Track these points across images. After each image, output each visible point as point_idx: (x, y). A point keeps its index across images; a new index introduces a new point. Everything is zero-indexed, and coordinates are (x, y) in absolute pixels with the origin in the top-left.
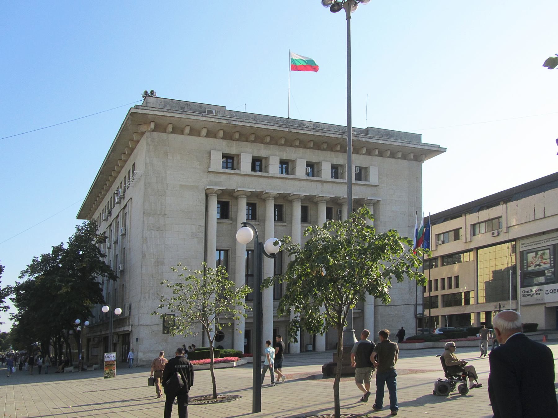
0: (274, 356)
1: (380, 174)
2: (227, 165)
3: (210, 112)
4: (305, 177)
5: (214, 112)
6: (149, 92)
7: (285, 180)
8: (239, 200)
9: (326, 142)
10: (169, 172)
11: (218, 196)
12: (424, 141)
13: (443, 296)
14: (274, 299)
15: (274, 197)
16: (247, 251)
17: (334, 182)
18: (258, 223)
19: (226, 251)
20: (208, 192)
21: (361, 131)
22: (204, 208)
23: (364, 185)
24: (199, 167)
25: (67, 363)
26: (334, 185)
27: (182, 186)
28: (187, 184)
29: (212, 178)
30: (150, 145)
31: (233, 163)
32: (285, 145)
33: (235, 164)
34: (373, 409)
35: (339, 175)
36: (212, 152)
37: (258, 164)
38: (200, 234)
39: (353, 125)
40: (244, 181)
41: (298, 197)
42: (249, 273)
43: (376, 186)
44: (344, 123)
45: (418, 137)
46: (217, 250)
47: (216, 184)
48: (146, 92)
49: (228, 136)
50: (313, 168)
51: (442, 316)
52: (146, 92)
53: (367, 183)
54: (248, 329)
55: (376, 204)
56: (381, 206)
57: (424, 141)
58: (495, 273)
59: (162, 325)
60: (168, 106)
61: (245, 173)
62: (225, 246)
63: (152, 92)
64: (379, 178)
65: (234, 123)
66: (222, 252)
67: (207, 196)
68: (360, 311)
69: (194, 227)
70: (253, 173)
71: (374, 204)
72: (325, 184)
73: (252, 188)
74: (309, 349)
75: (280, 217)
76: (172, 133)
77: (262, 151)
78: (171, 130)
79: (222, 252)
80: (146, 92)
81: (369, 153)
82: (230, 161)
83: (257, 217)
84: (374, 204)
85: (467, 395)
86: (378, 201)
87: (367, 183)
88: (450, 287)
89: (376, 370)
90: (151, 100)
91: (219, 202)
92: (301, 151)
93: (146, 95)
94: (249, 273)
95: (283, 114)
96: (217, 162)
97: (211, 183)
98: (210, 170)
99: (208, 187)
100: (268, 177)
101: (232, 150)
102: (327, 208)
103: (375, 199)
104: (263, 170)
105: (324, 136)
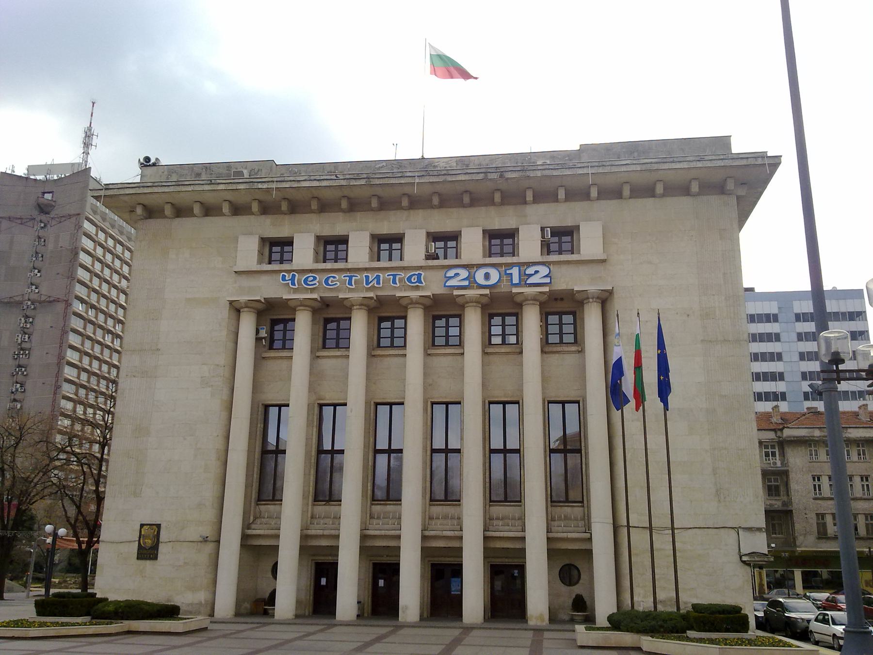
3: (240, 174)
9: (466, 191)
20: (238, 306)
21: (568, 156)
22: (223, 334)
29: (246, 282)
32: (503, 203)
34: (608, 625)
43: (603, 261)
45: (724, 142)
48: (147, 159)
49: (267, 209)
53: (574, 257)
55: (605, 299)
56: (617, 304)
65: (260, 186)
76: (598, 198)
77: (501, 220)
78: (662, 191)
82: (277, 248)
85: (444, 647)
86: (610, 293)
87: (574, 257)
89: (80, 591)
92: (419, 216)
96: (248, 252)
103: (592, 288)
105: (445, 182)
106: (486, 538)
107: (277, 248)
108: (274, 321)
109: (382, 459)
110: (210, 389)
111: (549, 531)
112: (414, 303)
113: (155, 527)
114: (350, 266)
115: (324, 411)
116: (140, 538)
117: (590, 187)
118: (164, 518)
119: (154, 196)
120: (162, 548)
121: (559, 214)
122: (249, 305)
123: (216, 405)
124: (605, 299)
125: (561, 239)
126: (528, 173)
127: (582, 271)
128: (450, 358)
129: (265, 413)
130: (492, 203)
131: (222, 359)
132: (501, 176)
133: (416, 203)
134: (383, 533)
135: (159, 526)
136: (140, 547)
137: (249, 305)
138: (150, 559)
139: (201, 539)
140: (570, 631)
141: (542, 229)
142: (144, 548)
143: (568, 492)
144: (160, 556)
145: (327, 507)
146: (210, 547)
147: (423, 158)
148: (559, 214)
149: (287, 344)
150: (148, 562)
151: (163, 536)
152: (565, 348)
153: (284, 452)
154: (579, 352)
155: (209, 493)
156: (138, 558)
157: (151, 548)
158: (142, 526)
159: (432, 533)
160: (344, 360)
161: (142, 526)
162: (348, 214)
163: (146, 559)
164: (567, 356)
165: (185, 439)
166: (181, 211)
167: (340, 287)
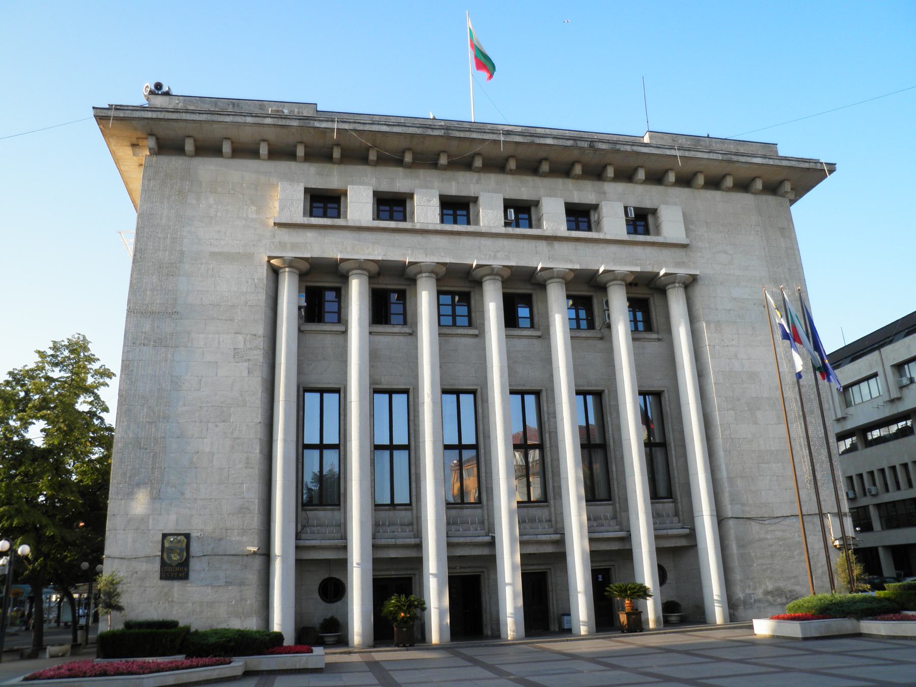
0: (199, 659)
4: (503, 230)
7: (457, 238)
15: (684, 283)
16: (643, 393)
18: (539, 333)
19: (598, 395)
26: (581, 247)
28: (226, 250)
35: (593, 226)
37: (391, 205)
38: (255, 352)
40: (357, 240)
41: (492, 272)
43: (684, 246)
47: (294, 246)
49: (320, 154)
58: (30, 440)
59: (158, 560)
61: (357, 224)
62: (655, 385)
64: (687, 230)
66: (590, 399)
67: (275, 272)
69: (240, 338)
72: (557, 245)
77: (584, 193)
81: (656, 178)
82: (324, 203)
83: (655, 325)
92: (492, 179)
103: (682, 271)
106: (298, 548)
107: (324, 203)
109: (312, 457)
110: (246, 364)
111: (374, 538)
113: (182, 538)
115: (597, 396)
116: (162, 551)
117: (368, 150)
118: (197, 526)
119: (181, 124)
120: (194, 565)
123: (256, 384)
124: (689, 283)
125: (641, 221)
126: (618, 147)
127: (666, 253)
128: (525, 341)
130: (435, 165)
131: (260, 329)
132: (591, 146)
133: (563, 170)
134: (468, 540)
135: (187, 536)
136: (163, 564)
137: (292, 263)
140: (746, 627)
141: (626, 208)
142: (171, 565)
143: (667, 486)
144: (192, 575)
145: (391, 513)
147: (708, 137)
148: (641, 195)
149: (408, 321)
151: (195, 548)
152: (460, 331)
154: (411, 334)
155: (253, 494)
156: (161, 578)
157: (180, 565)
158: (165, 536)
159: (308, 543)
160: (341, 337)
161: (165, 536)
162: (408, 170)
164: (646, 344)
165: (217, 426)
166: (209, 149)
167: (537, 258)
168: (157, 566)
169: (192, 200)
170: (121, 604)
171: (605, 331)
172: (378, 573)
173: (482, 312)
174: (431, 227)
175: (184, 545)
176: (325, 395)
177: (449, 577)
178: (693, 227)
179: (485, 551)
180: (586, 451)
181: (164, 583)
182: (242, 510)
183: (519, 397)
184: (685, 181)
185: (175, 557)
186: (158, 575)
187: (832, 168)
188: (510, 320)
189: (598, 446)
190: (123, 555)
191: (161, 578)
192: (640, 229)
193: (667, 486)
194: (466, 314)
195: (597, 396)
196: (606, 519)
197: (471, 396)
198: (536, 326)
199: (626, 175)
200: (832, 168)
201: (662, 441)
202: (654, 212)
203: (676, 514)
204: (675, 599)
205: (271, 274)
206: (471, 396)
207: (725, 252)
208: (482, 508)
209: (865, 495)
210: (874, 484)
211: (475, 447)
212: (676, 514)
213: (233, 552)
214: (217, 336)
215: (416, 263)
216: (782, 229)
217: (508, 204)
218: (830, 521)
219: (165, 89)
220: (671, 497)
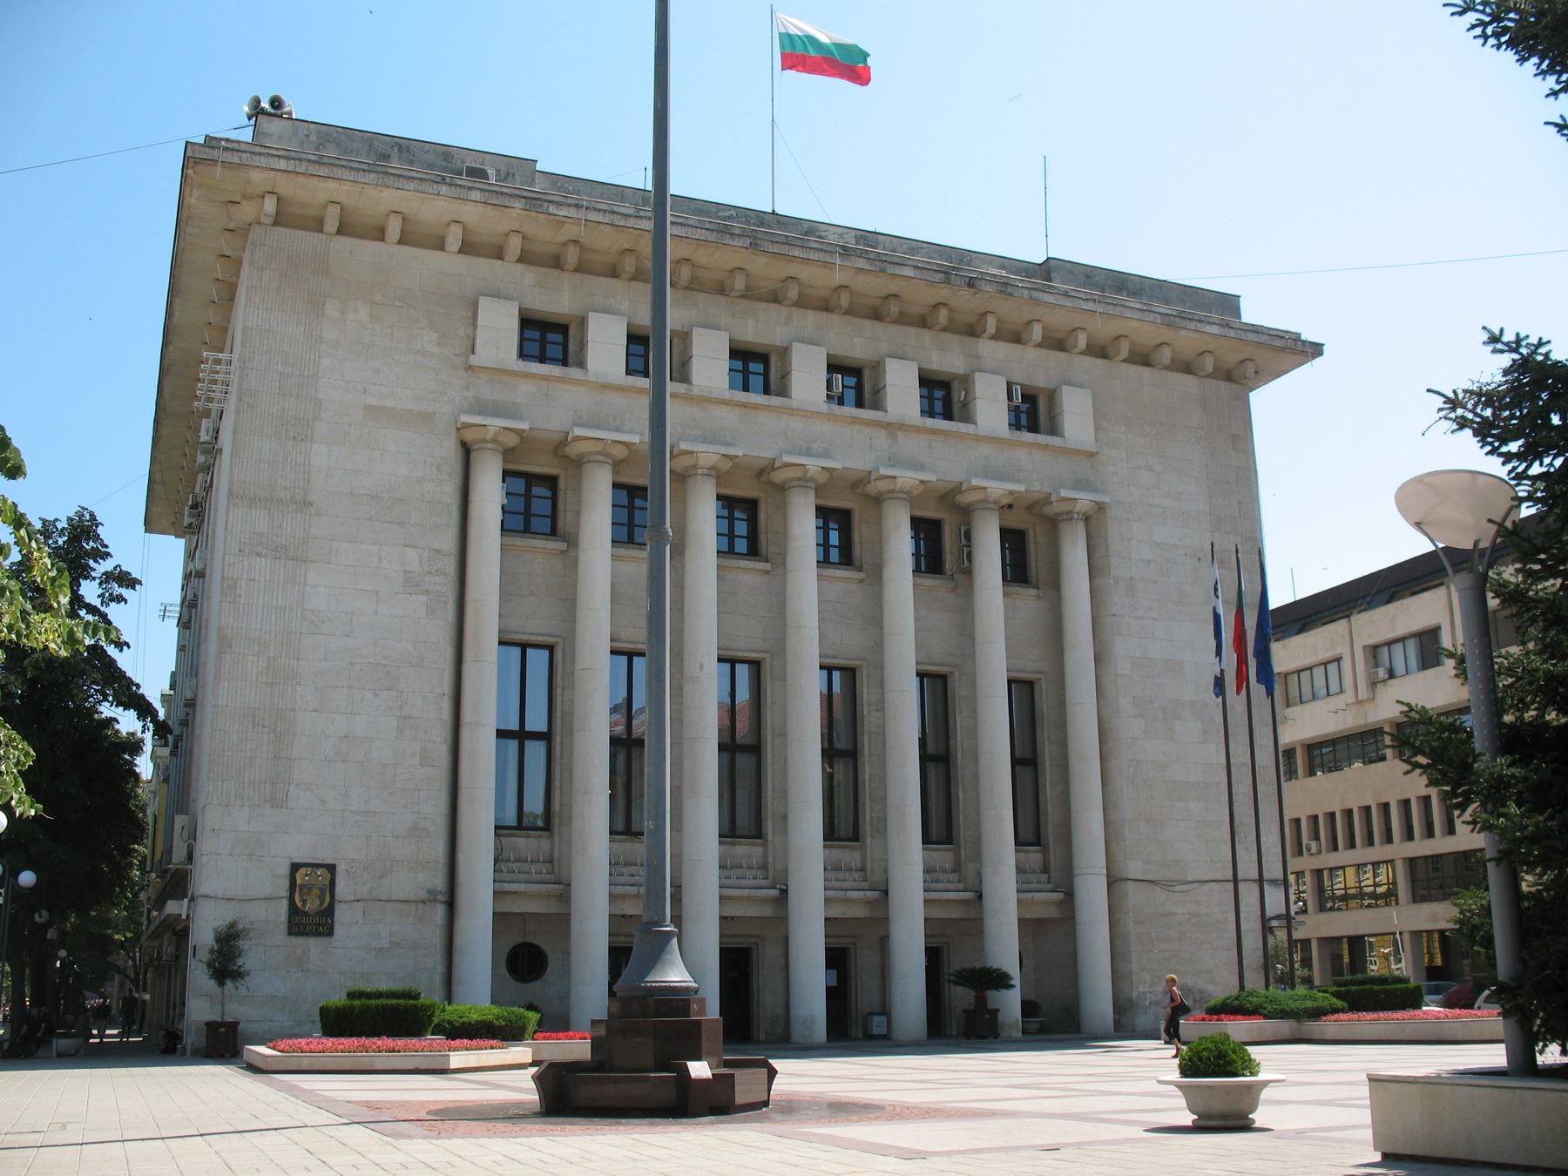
1: (1099, 416)
2: (931, 405)
3: (482, 174)
5: (491, 172)
6: (265, 105)
8: (587, 468)
10: (325, 362)
11: (508, 453)
12: (1249, 315)
13: (1412, 862)
14: (926, 840)
15: (712, 468)
17: (934, 432)
19: (756, 666)
20: (470, 436)
22: (451, 490)
23: (1046, 447)
24: (436, 350)
25: (752, 1019)
27: (371, 410)
28: (389, 403)
30: (262, 269)
31: (766, 375)
33: (572, 348)
36: (484, 303)
39: (676, 187)
42: (931, 750)
43: (1092, 455)
44: (640, 177)
45: (1228, 304)
46: (720, 660)
47: (498, 411)
50: (943, 396)
51: (1412, 933)
52: (256, 102)
53: (1055, 441)
54: (838, 943)
55: (1093, 521)
57: (1249, 315)
59: (285, 903)
60: (331, 147)
62: (748, 642)
63: (276, 102)
64: (1097, 427)
67: (467, 450)
68: (1061, 896)
69: (412, 554)
70: (741, 396)
71: (1086, 519)
73: (631, 432)
74: (876, 1031)
75: (930, 560)
77: (948, 358)
79: (836, 675)
80: (256, 102)
81: (1057, 343)
82: (548, 339)
83: (857, 551)
84: (1086, 519)
88: (1429, 833)
90: (273, 126)
91: (719, 497)
92: (809, 320)
93: (257, 111)
94: (931, 750)
95: (760, 202)
96: (499, 332)
97: (481, 408)
98: (474, 360)
99: (465, 418)
100: (791, 412)
101: (558, 300)
102: (1005, 532)
104: (570, 361)
107: (548, 339)
108: (538, 503)
110: (424, 598)
112: (804, 481)
114: (696, 391)
115: (752, 670)
118: (346, 852)
120: (342, 914)
121: (1035, 366)
122: (500, 438)
123: (439, 632)
125: (1032, 412)
129: (541, 652)
131: (449, 541)
135: (331, 868)
136: (293, 910)
138: (318, 934)
139: (423, 895)
141: (1009, 386)
142: (307, 914)
143: (1040, 827)
144: (338, 930)
145: (628, 846)
146: (440, 911)
147: (773, 213)
150: (312, 942)
153: (501, 734)
156: (290, 933)
158: (295, 867)
161: (295, 867)
163: (308, 934)
165: (376, 695)
168: (283, 909)
169: (332, 310)
170: (247, 967)
171: (959, 577)
172: (616, 939)
173: (784, 535)
174: (716, 394)
175: (327, 882)
176: (529, 651)
177: (610, 948)
178: (1105, 424)
179: (767, 911)
180: (726, 756)
181: (294, 940)
182: (417, 831)
183: (517, 651)
184: (1099, 351)
185: (312, 905)
186: (284, 927)
187: (1316, 350)
188: (627, 532)
189: (745, 751)
190: (229, 894)
191: (290, 933)
192: (756, 381)
193: (1040, 827)
194: (549, 512)
195: (752, 670)
196: (944, 871)
197: (546, 653)
198: (856, 562)
199: (1014, 336)
200: (1316, 350)
201: (850, 747)
202: (1052, 395)
203: (1045, 869)
204: (1032, 997)
205: (459, 448)
206: (546, 653)
207: (1150, 469)
208: (551, 837)
209: (1300, 853)
210: (1317, 838)
211: (546, 737)
212: (957, 869)
213: (402, 897)
214: (376, 548)
215: (691, 453)
216: (1235, 437)
217: (834, 367)
218: (1249, 895)
219: (1509, 337)
220: (1038, 844)
